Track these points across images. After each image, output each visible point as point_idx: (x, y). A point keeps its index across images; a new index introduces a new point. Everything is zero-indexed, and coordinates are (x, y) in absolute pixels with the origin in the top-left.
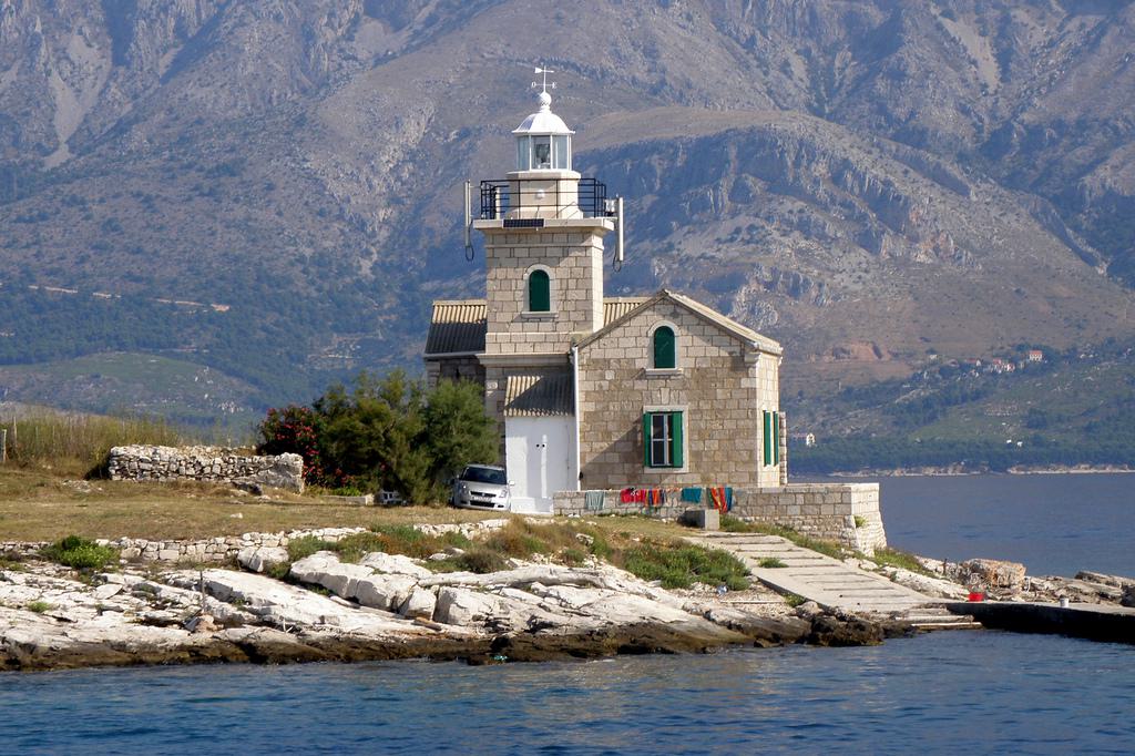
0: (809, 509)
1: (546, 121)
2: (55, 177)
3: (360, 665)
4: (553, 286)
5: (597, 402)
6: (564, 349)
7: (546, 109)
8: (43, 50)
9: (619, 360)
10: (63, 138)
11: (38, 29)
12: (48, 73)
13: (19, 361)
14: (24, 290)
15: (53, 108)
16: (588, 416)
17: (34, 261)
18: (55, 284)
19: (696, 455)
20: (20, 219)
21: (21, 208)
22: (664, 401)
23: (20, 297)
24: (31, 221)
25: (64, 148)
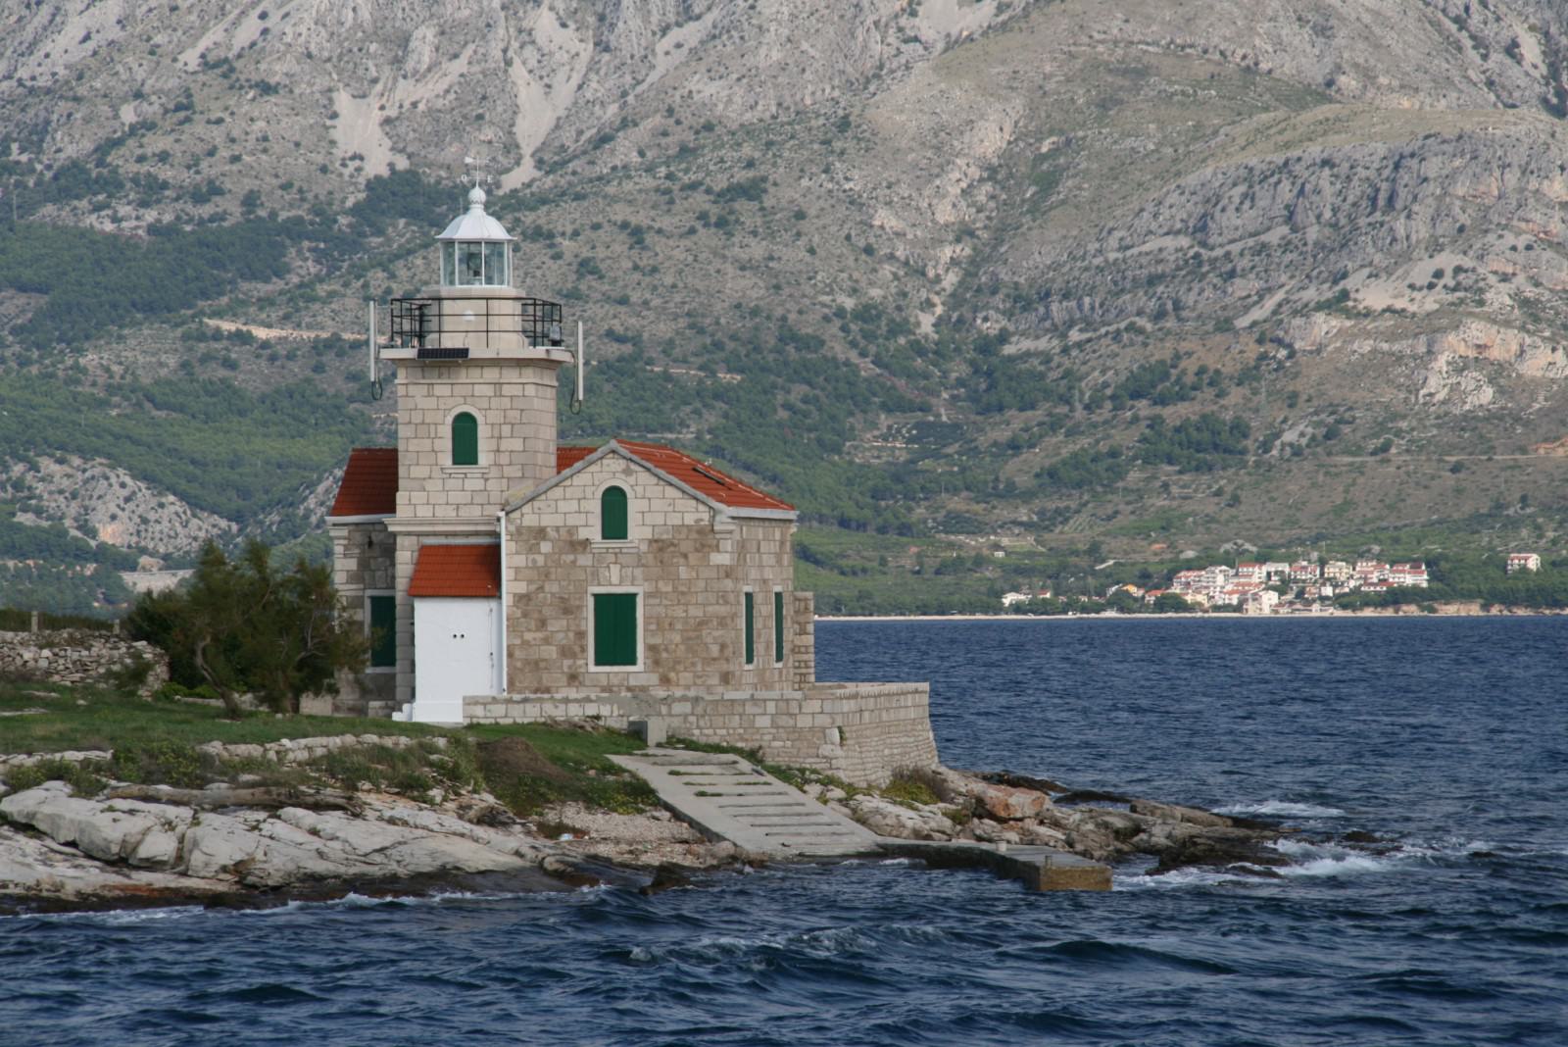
4: (483, 432)
5: (530, 582)
9: (557, 529)
19: (651, 648)
22: (615, 579)
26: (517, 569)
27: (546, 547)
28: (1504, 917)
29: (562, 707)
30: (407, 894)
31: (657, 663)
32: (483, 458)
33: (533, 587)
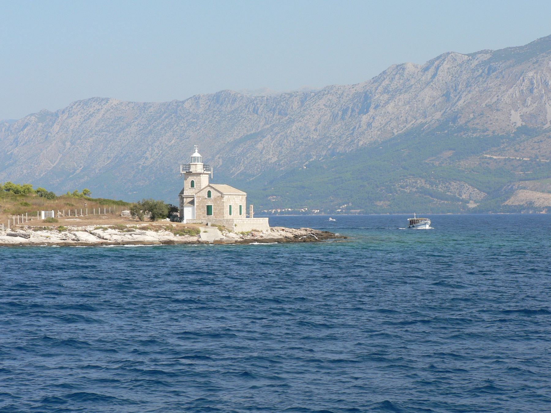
1: (196, 154)
2: (546, 131)
7: (196, 152)
8: (544, 98)
10: (548, 121)
11: (543, 92)
12: (545, 104)
13: (533, 180)
14: (535, 161)
15: (546, 113)
16: (197, 206)
17: (538, 153)
18: (543, 159)
19: (214, 213)
20: (535, 142)
21: (536, 139)
23: (534, 162)
24: (538, 142)
25: (549, 123)
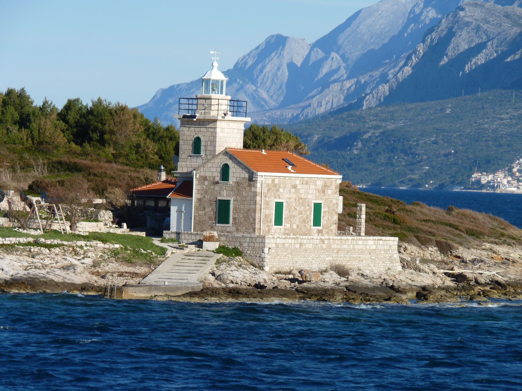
0: (251, 244)
3: (424, 354)
4: (203, 143)
5: (202, 194)
6: (190, 170)
7: (215, 68)
9: (210, 177)
16: (199, 200)
19: (234, 219)
22: (225, 195)
26: (198, 190)
27: (206, 183)
28: (409, 333)
29: (190, 236)
30: (93, 296)
31: (235, 223)
32: (202, 153)
33: (202, 196)
